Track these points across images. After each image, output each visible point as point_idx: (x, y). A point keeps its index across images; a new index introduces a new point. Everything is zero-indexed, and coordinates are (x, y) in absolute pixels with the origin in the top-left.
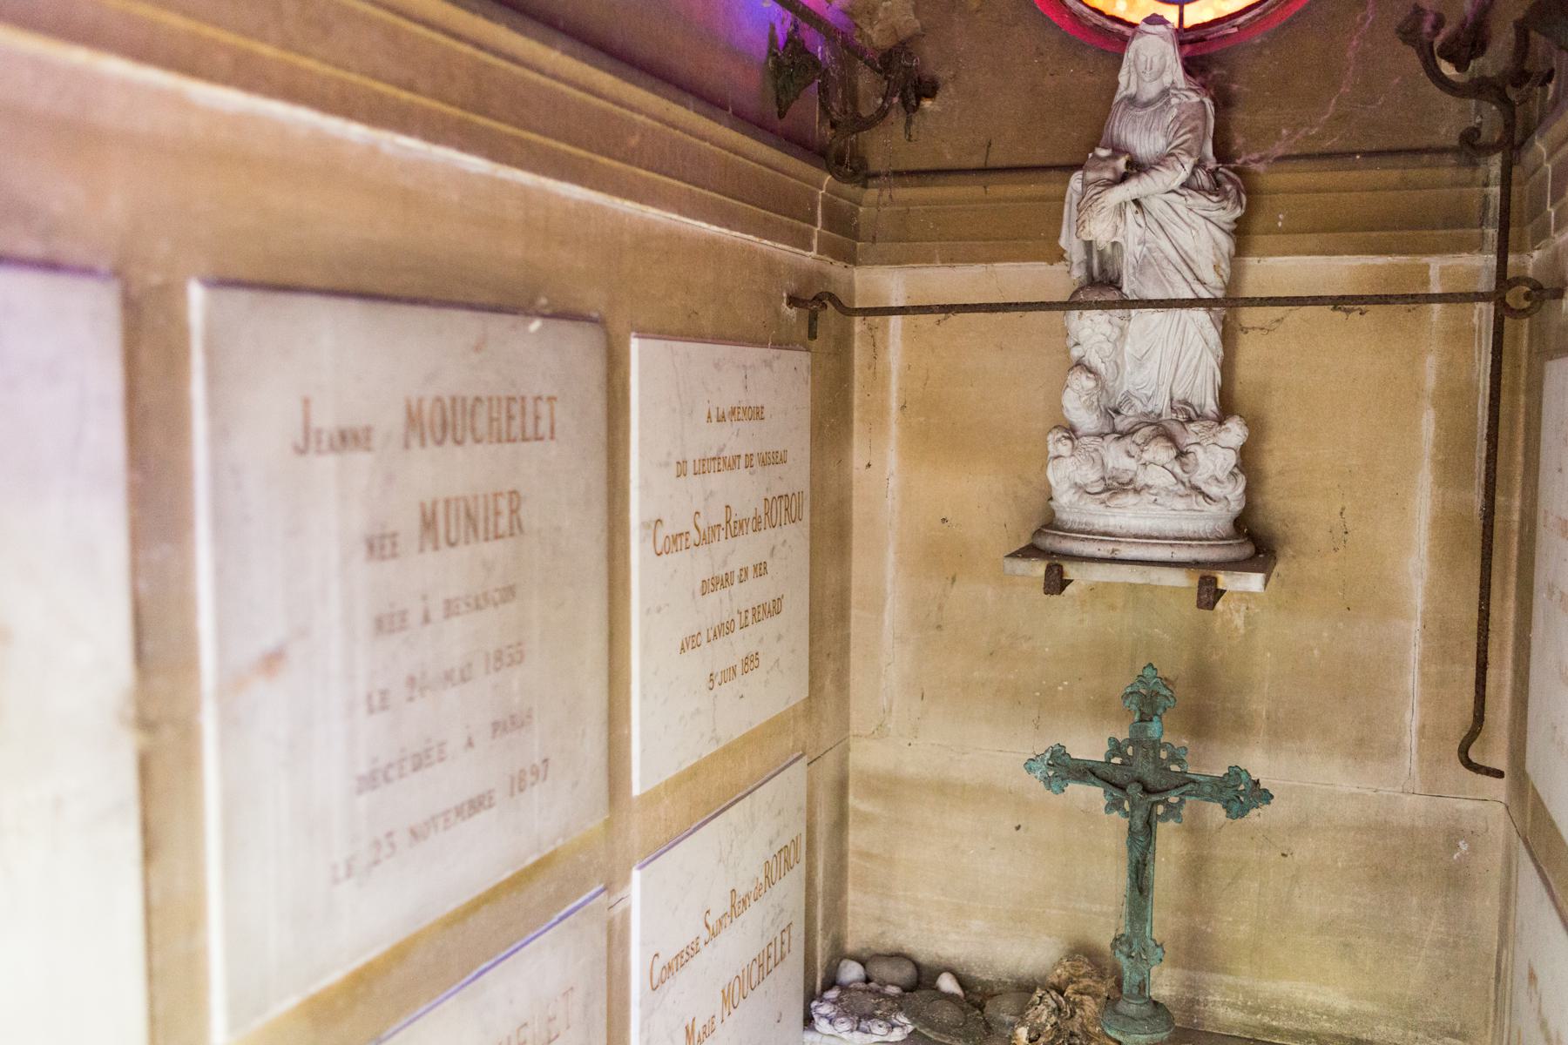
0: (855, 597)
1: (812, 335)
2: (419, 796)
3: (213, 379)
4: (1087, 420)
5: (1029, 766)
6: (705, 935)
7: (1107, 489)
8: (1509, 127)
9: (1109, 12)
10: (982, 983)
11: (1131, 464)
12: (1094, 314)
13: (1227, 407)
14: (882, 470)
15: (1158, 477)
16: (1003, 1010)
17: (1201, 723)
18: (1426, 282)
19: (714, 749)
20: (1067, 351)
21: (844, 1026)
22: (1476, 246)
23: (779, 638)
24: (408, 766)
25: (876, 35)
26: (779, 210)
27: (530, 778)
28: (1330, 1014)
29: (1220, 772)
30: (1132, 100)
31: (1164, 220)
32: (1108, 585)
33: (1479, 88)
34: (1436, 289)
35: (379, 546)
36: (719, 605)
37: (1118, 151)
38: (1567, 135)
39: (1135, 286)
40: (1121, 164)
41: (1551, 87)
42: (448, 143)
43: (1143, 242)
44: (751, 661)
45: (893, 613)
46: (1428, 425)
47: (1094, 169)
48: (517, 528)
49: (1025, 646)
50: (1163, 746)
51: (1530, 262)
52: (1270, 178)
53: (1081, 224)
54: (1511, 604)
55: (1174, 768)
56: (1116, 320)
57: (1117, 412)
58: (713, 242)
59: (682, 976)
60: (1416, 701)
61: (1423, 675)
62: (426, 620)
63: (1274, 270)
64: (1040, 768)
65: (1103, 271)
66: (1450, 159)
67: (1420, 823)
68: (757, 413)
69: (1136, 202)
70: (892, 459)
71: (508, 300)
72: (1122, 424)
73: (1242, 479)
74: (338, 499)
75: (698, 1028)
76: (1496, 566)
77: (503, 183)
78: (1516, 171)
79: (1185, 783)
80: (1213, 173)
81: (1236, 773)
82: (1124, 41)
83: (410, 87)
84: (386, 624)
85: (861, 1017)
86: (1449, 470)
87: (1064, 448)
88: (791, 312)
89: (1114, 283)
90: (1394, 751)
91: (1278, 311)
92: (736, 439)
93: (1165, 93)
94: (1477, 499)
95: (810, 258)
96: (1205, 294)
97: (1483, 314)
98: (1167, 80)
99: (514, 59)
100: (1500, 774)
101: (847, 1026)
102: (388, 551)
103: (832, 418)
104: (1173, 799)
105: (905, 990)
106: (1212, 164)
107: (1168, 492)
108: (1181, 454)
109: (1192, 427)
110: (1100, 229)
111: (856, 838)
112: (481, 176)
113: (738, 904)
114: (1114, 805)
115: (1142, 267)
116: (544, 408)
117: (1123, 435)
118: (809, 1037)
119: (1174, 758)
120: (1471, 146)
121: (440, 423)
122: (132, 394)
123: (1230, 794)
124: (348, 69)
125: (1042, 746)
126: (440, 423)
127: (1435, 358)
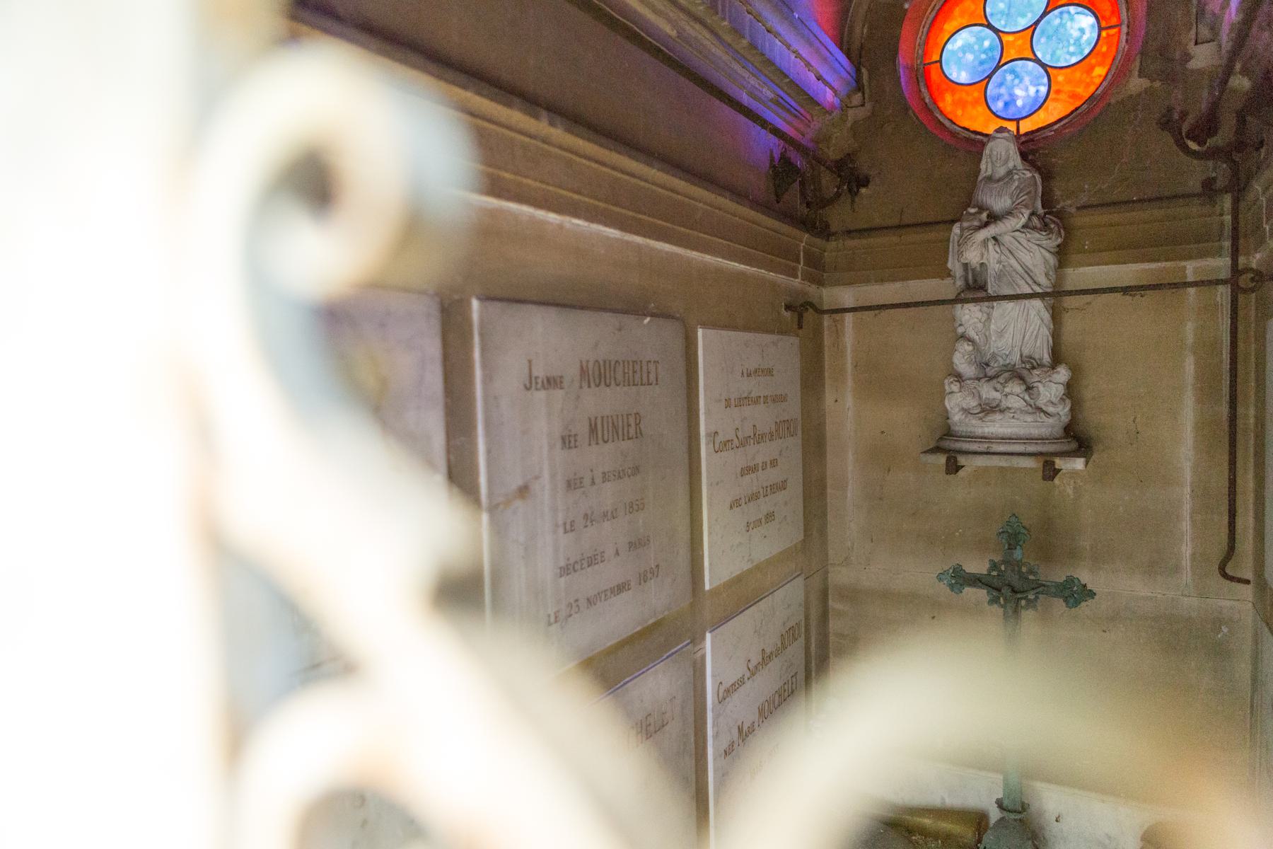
0: (829, 482)
1: (800, 327)
2: (589, 581)
3: (484, 350)
4: (967, 369)
6: (748, 674)
8: (1235, 173)
9: (972, 128)
11: (997, 395)
12: (971, 306)
13: (1057, 358)
14: (846, 410)
15: (1015, 402)
17: (1047, 553)
19: (749, 566)
20: (955, 330)
22: (1218, 253)
23: (786, 503)
24: (585, 565)
25: (833, 154)
26: (781, 256)
27: (649, 575)
29: (1062, 579)
30: (989, 179)
31: (1013, 248)
32: (986, 469)
33: (1213, 154)
34: (1190, 278)
35: (568, 441)
36: (751, 483)
37: (981, 209)
38: (1272, 180)
40: (984, 216)
41: (1263, 151)
42: (599, 222)
43: (999, 262)
44: (770, 517)
45: (853, 491)
46: (1190, 365)
48: (639, 434)
50: (1024, 564)
51: (1255, 260)
52: (1081, 220)
53: (960, 254)
54: (1251, 475)
55: (1031, 577)
56: (985, 309)
57: (987, 365)
58: (743, 273)
59: (736, 696)
60: (1188, 541)
61: (1193, 521)
62: (593, 483)
63: (1083, 274)
65: (975, 281)
66: (1196, 201)
67: (1194, 615)
68: (769, 372)
69: (994, 238)
70: (849, 400)
71: (632, 306)
72: (990, 372)
73: (1068, 402)
74: (543, 420)
75: (745, 728)
76: (1240, 454)
77: (627, 242)
78: (1242, 205)
79: (1039, 587)
80: (1042, 218)
81: (1071, 581)
82: (983, 145)
83: (578, 193)
84: (572, 484)
86: (1205, 390)
87: (955, 387)
88: (787, 314)
89: (983, 287)
92: (754, 387)
93: (1010, 173)
94: (1224, 410)
95: (797, 283)
96: (1039, 290)
97: (1223, 293)
98: (1011, 165)
99: (632, 175)
100: (1248, 582)
102: (572, 444)
103: (813, 378)
104: (1031, 597)
106: (1041, 211)
107: (1022, 411)
108: (1029, 389)
109: (1036, 372)
110: (973, 256)
111: (834, 625)
112: (617, 240)
113: (766, 658)
114: (994, 601)
115: (999, 277)
116: (652, 367)
117: (991, 378)
119: (1031, 572)
120: (1209, 190)
121: (598, 374)
122: (446, 357)
123: (1067, 593)
124: (548, 184)
125: (948, 566)
126: (598, 374)
127: (1195, 322)
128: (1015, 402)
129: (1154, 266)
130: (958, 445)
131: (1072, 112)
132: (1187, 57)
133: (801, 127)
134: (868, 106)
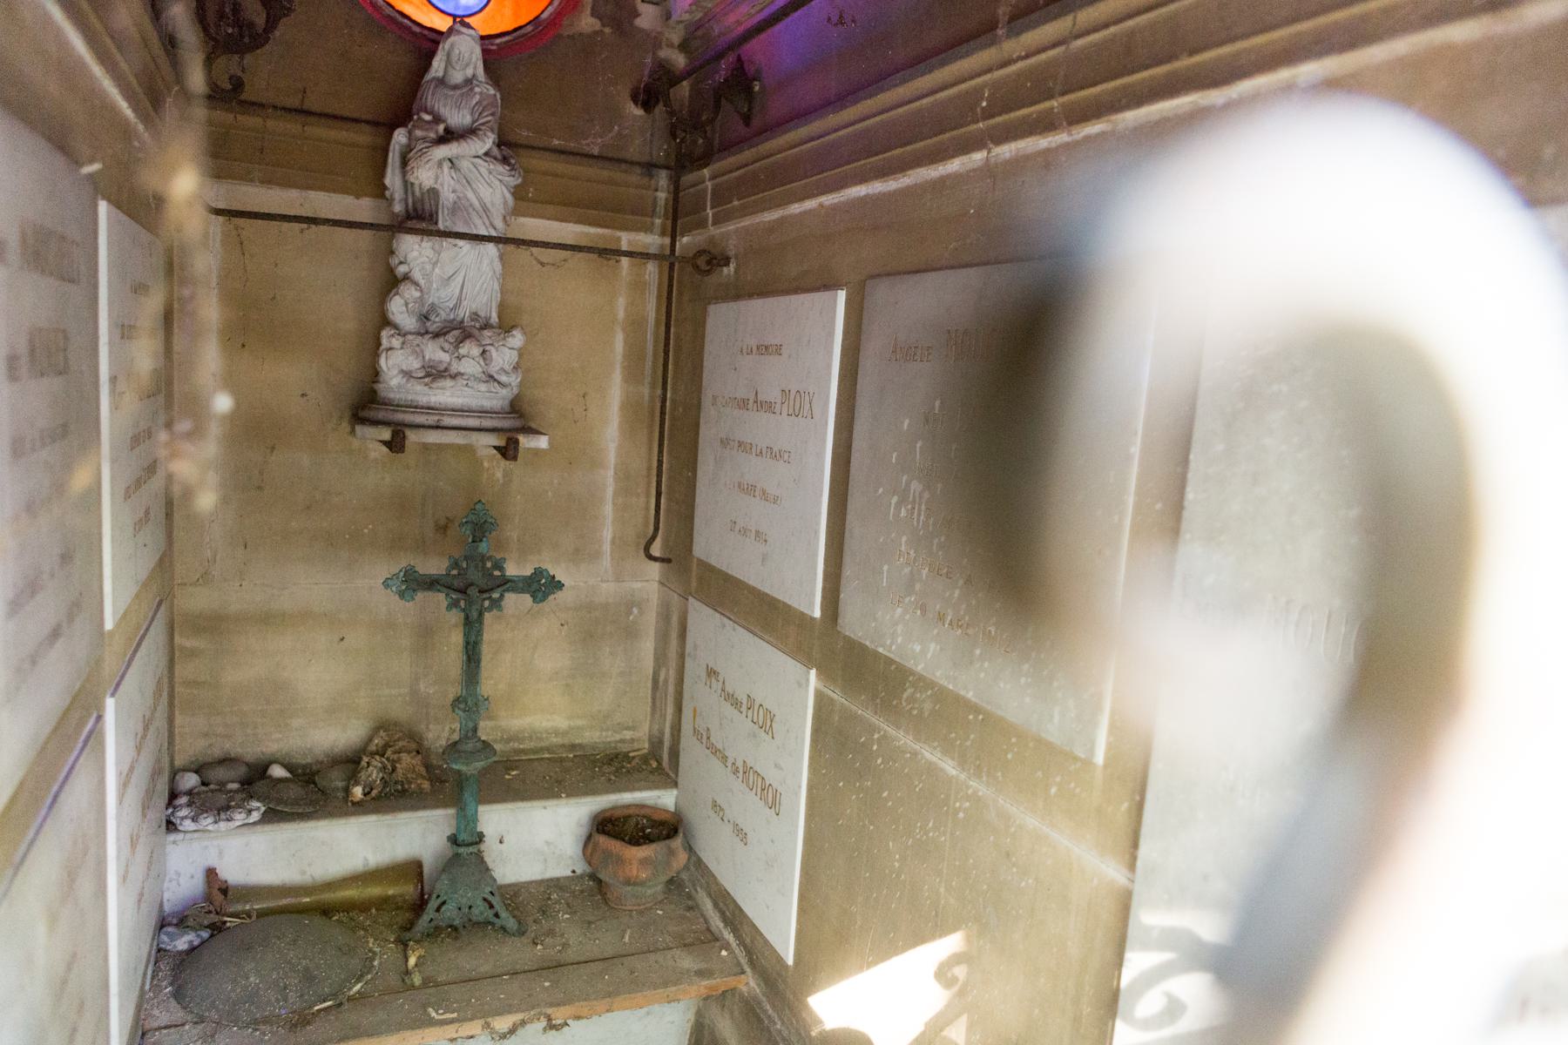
5: (386, 584)
7: (428, 375)
11: (445, 357)
16: (336, 780)
21: (207, 821)
28: (557, 733)
30: (441, 82)
34: (624, 248)
37: (438, 119)
39: (448, 224)
40: (441, 128)
50: (490, 558)
55: (497, 573)
65: (415, 209)
66: (638, 170)
72: (433, 328)
79: (506, 584)
81: (539, 573)
85: (222, 811)
89: (432, 218)
90: (596, 556)
96: (494, 234)
98: (469, 72)
101: (210, 820)
105: (242, 784)
109: (487, 333)
110: (424, 176)
114: (454, 604)
115: (455, 209)
117: (436, 335)
118: (172, 837)
123: (535, 586)
130: (400, 417)
131: (516, 30)
132: (637, 14)
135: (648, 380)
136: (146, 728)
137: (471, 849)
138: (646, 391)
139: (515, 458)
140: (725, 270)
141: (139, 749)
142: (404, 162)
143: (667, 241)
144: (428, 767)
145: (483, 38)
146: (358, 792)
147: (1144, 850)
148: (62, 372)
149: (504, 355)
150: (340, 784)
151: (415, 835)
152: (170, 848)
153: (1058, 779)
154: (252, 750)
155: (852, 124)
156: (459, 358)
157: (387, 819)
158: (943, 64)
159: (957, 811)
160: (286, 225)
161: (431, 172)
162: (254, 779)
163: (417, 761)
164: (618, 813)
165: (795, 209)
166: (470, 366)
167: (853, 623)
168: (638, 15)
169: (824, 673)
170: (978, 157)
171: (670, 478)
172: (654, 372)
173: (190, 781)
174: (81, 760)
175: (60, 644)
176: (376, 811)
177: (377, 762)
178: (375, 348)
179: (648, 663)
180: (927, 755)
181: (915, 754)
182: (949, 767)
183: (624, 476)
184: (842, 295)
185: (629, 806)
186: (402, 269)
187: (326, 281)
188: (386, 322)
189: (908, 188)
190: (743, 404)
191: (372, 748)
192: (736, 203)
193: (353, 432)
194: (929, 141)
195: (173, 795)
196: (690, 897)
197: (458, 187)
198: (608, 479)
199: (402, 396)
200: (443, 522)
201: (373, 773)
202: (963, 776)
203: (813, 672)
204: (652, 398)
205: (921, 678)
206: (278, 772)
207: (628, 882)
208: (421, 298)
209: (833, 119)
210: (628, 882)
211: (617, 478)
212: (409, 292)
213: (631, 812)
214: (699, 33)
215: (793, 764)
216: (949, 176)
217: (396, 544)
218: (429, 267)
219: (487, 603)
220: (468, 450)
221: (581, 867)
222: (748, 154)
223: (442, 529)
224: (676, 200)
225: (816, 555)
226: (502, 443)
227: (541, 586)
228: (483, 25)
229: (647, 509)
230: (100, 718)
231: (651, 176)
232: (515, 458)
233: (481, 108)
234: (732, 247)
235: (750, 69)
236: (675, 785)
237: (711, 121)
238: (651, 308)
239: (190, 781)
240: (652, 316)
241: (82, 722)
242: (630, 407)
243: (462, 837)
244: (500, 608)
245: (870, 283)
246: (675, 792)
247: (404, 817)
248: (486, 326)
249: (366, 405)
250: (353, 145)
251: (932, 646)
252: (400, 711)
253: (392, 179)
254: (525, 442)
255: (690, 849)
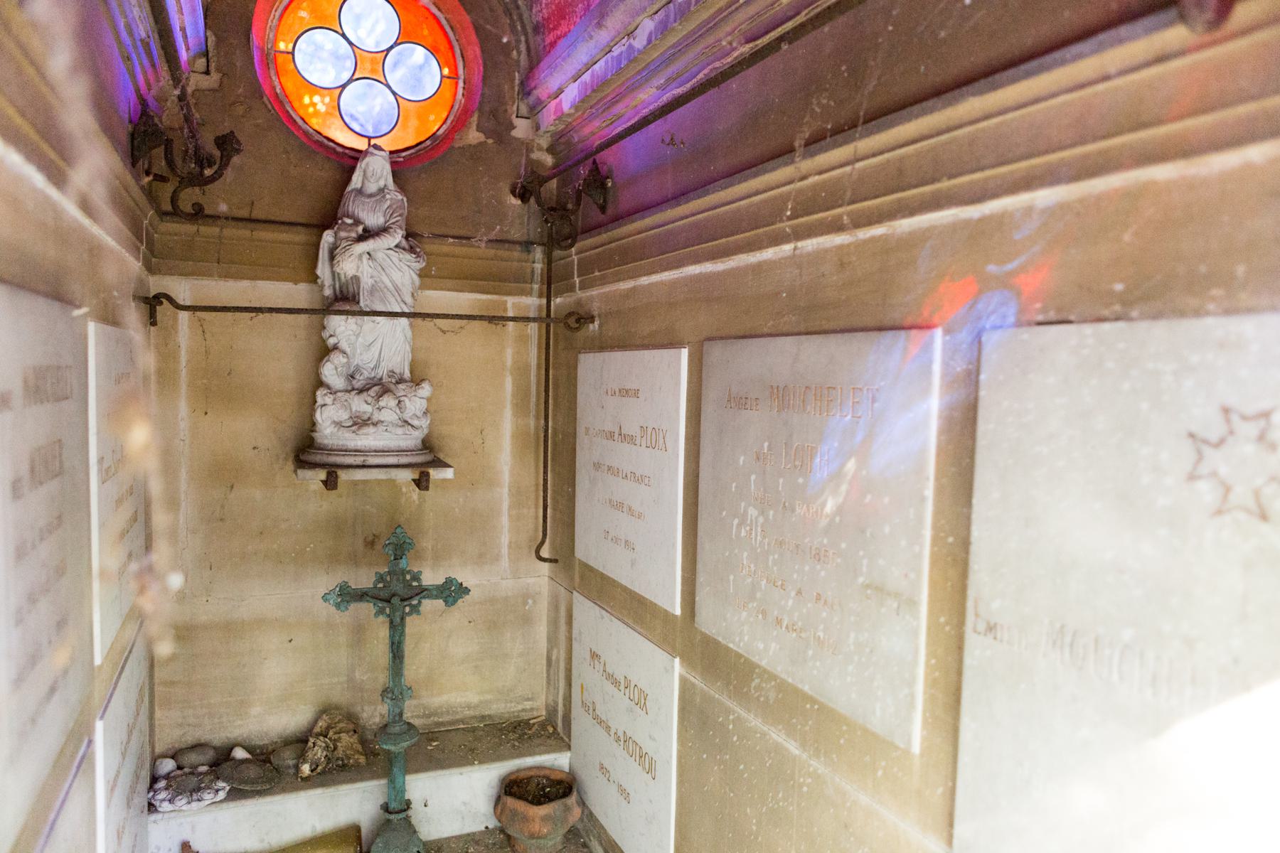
5: (325, 598)
7: (355, 424)
10: (260, 747)
11: (369, 409)
16: (288, 758)
18: (505, 310)
21: (181, 802)
30: (360, 192)
34: (510, 314)
37: (357, 222)
40: (360, 229)
47: (345, 230)
49: (283, 526)
50: (409, 572)
55: (415, 584)
61: (510, 516)
64: (334, 598)
66: (518, 247)
72: (357, 385)
79: (423, 592)
81: (449, 581)
83: (23, 115)
85: (194, 792)
89: (354, 299)
90: (497, 558)
91: (458, 322)
96: (407, 310)
98: (382, 183)
101: (184, 801)
109: (401, 386)
110: (348, 267)
112: (35, 190)
114: (381, 612)
115: (373, 291)
117: (361, 391)
118: (154, 817)
123: (447, 592)
127: (516, 350)
128: (388, 415)
129: (484, 297)
130: (333, 459)
133: (151, 78)
134: (215, 77)
135: (533, 413)
136: (130, 734)
137: (402, 816)
138: (532, 423)
139: (427, 488)
140: (591, 326)
141: (124, 755)
142: (332, 257)
143: (544, 301)
144: (363, 742)
145: (391, 152)
146: (306, 769)
147: (959, 829)
148: (59, 474)
149: (416, 403)
150: (291, 762)
151: (353, 803)
152: (151, 827)
153: (883, 764)
154: (219, 737)
155: (687, 217)
156: (380, 409)
157: (330, 791)
158: (755, 175)
159: (801, 786)
160: (238, 314)
161: (355, 263)
162: (221, 761)
163: (355, 739)
164: (522, 775)
165: (644, 281)
166: (388, 415)
167: (707, 621)
168: (514, 128)
169: (687, 661)
170: (787, 248)
171: (554, 491)
172: (537, 405)
173: (168, 765)
174: (75, 785)
175: (57, 697)
176: (323, 785)
177: (321, 742)
178: (313, 411)
179: (543, 645)
180: (774, 736)
181: (764, 734)
182: (793, 747)
183: (516, 492)
184: (685, 353)
185: (530, 768)
186: (331, 341)
187: (273, 353)
188: (320, 384)
189: (732, 269)
190: (611, 436)
191: (317, 730)
192: (597, 274)
193: (295, 471)
194: (747, 234)
195: (154, 780)
196: (585, 845)
197: (375, 273)
198: (504, 495)
199: (335, 442)
200: (371, 538)
201: (318, 752)
202: (805, 756)
203: (677, 660)
204: (537, 428)
205: (765, 671)
206: (240, 754)
207: (532, 836)
208: (348, 364)
209: (671, 213)
210: (532, 836)
211: (511, 494)
212: (337, 358)
213: (532, 773)
214: (562, 140)
215: (664, 735)
216: (765, 262)
217: (333, 559)
218: (353, 338)
219: (407, 609)
220: (391, 482)
221: (492, 823)
222: (604, 237)
223: (371, 543)
224: (549, 270)
225: (674, 563)
226: (417, 477)
227: (452, 592)
228: (387, 144)
229: (537, 518)
230: (90, 742)
231: (529, 252)
232: (427, 488)
233: (391, 211)
234: (595, 308)
235: (604, 170)
236: (569, 748)
237: (574, 212)
238: (533, 355)
239: (168, 765)
240: (533, 361)
241: (77, 748)
242: (519, 436)
243: (393, 806)
244: (418, 612)
245: (707, 345)
246: (568, 754)
247: (345, 788)
248: (401, 381)
249: (305, 450)
250: (289, 243)
251: (773, 645)
252: (339, 696)
253: (323, 270)
254: (435, 474)
255: (582, 803)
